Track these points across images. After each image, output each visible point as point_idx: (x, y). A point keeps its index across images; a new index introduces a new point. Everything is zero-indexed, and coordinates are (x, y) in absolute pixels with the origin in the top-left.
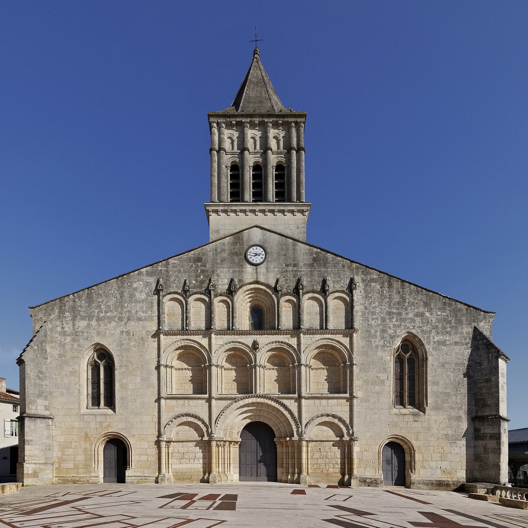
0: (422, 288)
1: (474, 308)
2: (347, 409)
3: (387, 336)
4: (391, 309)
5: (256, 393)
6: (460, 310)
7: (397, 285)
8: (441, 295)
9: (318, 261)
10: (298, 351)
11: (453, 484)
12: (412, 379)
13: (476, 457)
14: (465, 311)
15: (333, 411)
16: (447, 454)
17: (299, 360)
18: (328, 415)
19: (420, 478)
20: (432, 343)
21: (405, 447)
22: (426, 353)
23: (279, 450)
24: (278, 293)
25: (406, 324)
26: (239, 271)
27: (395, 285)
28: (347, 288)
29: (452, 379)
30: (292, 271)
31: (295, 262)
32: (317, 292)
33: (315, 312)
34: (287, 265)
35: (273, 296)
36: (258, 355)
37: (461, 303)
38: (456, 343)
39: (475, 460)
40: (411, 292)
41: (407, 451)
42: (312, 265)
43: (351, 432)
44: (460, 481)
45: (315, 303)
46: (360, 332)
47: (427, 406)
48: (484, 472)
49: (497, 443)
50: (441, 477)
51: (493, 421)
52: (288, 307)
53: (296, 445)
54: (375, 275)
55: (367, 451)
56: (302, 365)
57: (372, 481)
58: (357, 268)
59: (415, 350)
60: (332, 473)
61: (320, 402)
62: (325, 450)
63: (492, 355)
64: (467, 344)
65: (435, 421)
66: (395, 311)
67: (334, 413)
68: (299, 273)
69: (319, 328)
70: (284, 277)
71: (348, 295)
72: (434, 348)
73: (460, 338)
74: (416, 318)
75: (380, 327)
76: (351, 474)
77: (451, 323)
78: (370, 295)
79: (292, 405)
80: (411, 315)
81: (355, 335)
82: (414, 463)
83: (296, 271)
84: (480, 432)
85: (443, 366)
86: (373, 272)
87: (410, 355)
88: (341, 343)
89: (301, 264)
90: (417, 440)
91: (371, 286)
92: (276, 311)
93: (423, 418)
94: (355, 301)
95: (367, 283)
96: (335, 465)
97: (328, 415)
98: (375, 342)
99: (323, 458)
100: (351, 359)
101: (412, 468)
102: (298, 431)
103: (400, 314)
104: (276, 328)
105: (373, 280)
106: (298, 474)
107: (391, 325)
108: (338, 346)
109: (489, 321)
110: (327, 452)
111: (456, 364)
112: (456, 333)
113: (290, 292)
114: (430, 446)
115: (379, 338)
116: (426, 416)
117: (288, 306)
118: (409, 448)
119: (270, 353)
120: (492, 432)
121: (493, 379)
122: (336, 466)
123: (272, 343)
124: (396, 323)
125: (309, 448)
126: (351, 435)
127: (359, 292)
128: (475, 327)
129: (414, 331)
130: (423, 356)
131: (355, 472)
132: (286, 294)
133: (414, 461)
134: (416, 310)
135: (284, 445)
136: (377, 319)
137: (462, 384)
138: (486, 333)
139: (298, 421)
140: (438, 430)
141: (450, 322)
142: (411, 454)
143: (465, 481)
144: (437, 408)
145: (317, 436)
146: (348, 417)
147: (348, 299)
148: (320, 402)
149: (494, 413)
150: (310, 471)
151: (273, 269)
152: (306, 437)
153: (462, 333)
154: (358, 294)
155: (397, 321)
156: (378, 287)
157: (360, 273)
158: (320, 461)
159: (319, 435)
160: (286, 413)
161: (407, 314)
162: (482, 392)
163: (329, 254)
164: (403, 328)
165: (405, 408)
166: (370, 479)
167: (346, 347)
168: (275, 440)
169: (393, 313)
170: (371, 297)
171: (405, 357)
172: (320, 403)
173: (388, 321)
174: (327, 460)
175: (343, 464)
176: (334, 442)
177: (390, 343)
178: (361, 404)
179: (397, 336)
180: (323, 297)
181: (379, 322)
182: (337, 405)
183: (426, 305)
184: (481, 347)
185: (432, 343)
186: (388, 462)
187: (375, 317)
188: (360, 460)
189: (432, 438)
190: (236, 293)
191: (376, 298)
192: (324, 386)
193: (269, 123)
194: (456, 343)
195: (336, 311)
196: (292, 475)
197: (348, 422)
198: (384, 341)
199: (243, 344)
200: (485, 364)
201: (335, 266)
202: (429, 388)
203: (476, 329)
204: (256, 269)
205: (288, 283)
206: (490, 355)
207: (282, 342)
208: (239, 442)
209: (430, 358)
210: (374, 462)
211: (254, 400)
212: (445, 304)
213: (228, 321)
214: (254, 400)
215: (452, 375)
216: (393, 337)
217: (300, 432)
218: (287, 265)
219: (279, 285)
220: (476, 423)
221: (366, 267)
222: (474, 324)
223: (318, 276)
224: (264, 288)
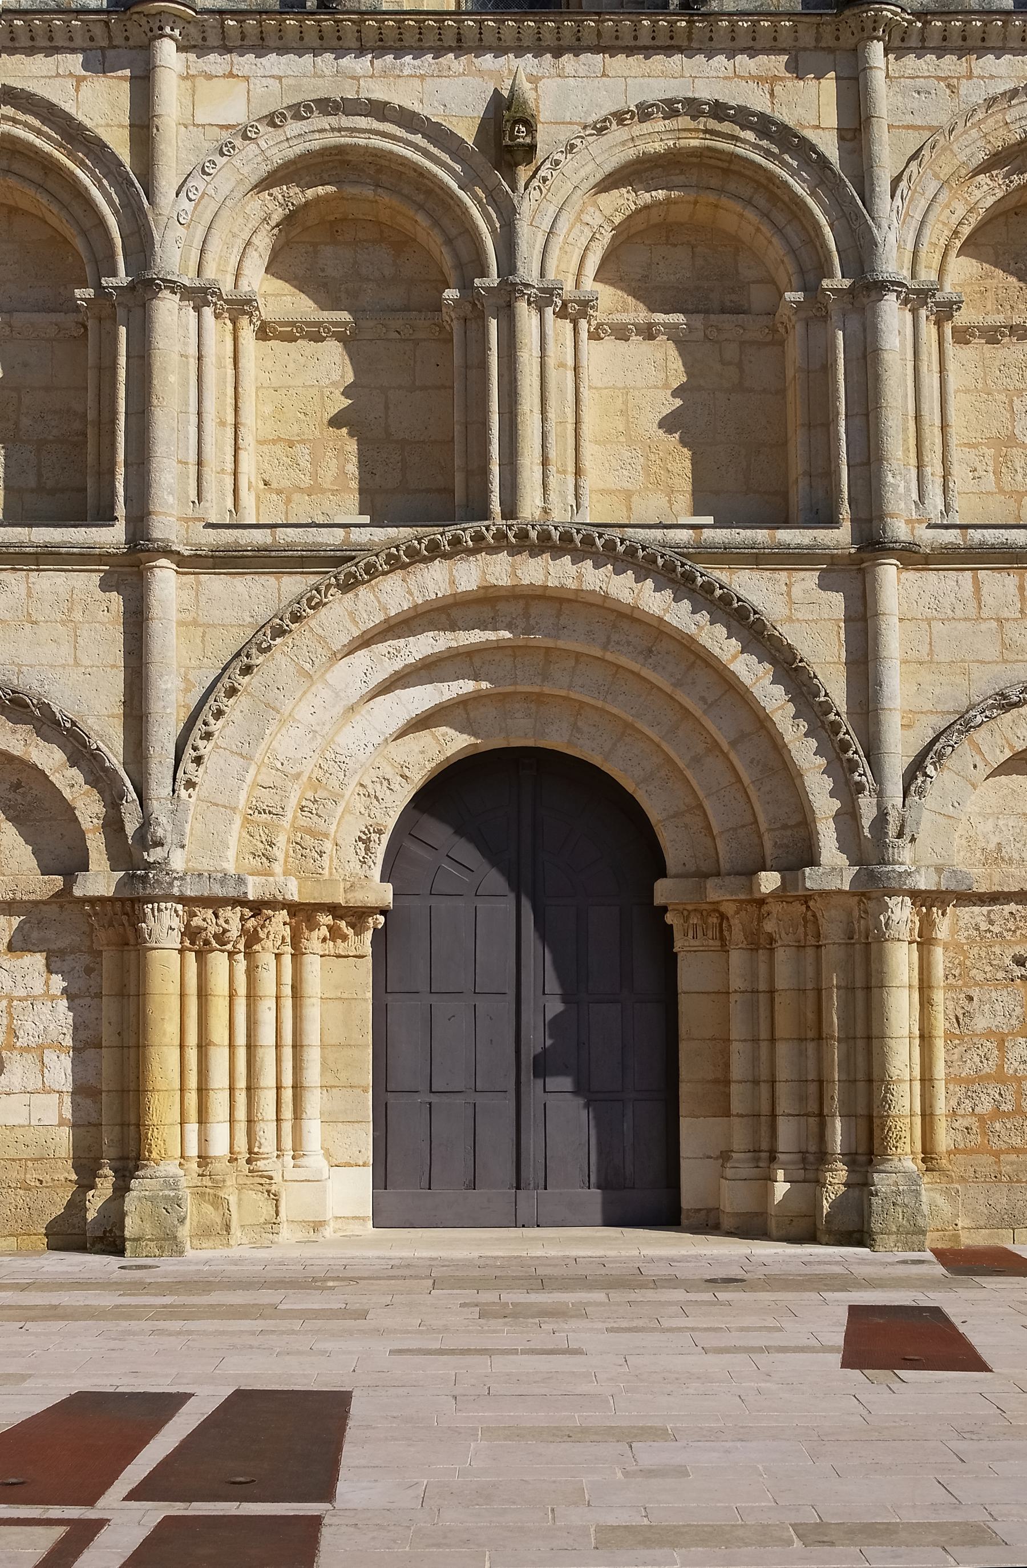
5: (510, 511)
56: (881, 287)
102: (113, 825)
106: (851, 1159)
125: (939, 954)
135: (737, 934)
145: (996, 857)
150: (944, 1140)
159: (1008, 851)
196: (800, 1174)
199: (408, 120)
217: (866, 823)
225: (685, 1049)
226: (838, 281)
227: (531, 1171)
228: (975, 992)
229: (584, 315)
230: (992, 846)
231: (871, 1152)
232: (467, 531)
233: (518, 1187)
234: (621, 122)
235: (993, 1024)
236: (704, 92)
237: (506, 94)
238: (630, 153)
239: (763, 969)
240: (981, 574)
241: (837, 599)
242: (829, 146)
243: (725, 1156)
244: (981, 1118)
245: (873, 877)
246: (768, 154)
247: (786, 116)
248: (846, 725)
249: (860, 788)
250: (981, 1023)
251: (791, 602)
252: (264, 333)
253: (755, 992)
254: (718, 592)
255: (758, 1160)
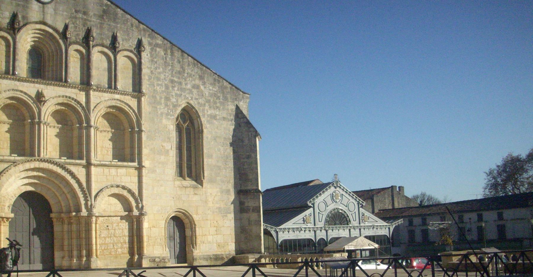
0: (198, 61)
1: (236, 88)
2: (136, 179)
3: (171, 104)
4: (173, 77)
5: (39, 156)
6: (226, 88)
7: (177, 54)
8: (211, 71)
9: (108, 14)
10: (87, 109)
11: (227, 257)
12: (189, 150)
13: (242, 229)
14: (229, 89)
15: (122, 182)
16: (221, 227)
17: (88, 121)
18: (118, 186)
19: (201, 254)
20: (206, 116)
21: (186, 221)
22: (202, 125)
23: (57, 228)
24: (67, 40)
25: (186, 94)
26: (23, 6)
27: (176, 54)
28: (135, 49)
29: (222, 153)
30: (82, 19)
31: (85, 10)
32: (107, 47)
33: (103, 68)
34: (76, 11)
35: (61, 41)
36: (44, 109)
37: (227, 81)
38: (224, 119)
39: (241, 232)
40: (189, 64)
41: (187, 225)
42: (101, 17)
43: (140, 205)
44: (231, 254)
45: (104, 58)
46: (147, 97)
47: (204, 179)
48: (249, 244)
49: (258, 215)
50: (217, 251)
51: (254, 195)
52: (75, 57)
53: (83, 221)
54: (159, 41)
55: (155, 227)
56: (91, 126)
57: (161, 260)
58: (144, 30)
59: (192, 122)
60: (120, 254)
61: (109, 171)
62: (112, 227)
63: (251, 134)
64: (231, 120)
65: (211, 194)
66: (176, 79)
67: (123, 184)
68: (88, 23)
69: (107, 86)
70: (73, 24)
71: (136, 56)
72: (208, 121)
73: (227, 114)
74: (193, 90)
75: (164, 94)
76: (141, 255)
77: (219, 99)
78: (155, 60)
79: (80, 173)
80: (189, 86)
81: (143, 99)
82: (196, 238)
83: (86, 20)
84: (244, 205)
85: (215, 139)
86: (158, 37)
87: (188, 126)
88: (129, 106)
89: (91, 14)
90: (197, 214)
91: (156, 51)
92: (64, 61)
93: (201, 191)
94: (143, 63)
95: (153, 47)
96: (123, 244)
97: (118, 186)
98: (160, 109)
99: (111, 237)
100: (139, 125)
101: (193, 244)
102: (86, 204)
103: (180, 83)
104: (64, 80)
105: (157, 45)
106: (86, 256)
107: (173, 94)
108: (127, 108)
109: (246, 101)
110: (115, 230)
111: (225, 138)
112: (223, 109)
113: (79, 42)
114: (208, 220)
115: (163, 105)
116: (204, 189)
117: (76, 57)
118: (190, 222)
119: (59, 107)
120: (254, 205)
121: (253, 155)
122: (125, 246)
123: (59, 96)
124: (177, 92)
125: (98, 225)
126: (141, 209)
127: (146, 55)
128: (237, 105)
129: (192, 102)
130: (199, 128)
131: (145, 251)
132: (76, 43)
133: (195, 236)
134: (193, 82)
135: (66, 222)
136: (161, 85)
137: (229, 159)
138: (245, 112)
139: (87, 191)
140: (213, 203)
141: (218, 98)
142: (192, 229)
143: (235, 253)
144: (211, 181)
145: (104, 211)
146: (137, 189)
147: (136, 59)
148: (109, 171)
149: (255, 188)
150: (98, 253)
151: (61, 12)
152: (96, 211)
153: (228, 110)
154: (145, 56)
155: (178, 90)
156: (162, 53)
157: (147, 36)
158: (108, 240)
159: (106, 210)
160: (73, 182)
161: (186, 84)
162: (245, 167)
163: (119, 10)
164: (183, 98)
165: (185, 180)
166: (159, 257)
167: (134, 111)
168: (52, 215)
169: (175, 82)
170: (156, 62)
171: (183, 127)
172: (110, 173)
173: (171, 88)
174: (115, 239)
175: (131, 242)
176: (89, 207)
177: (173, 112)
178: (148, 174)
179: (178, 105)
180: (113, 53)
181: (163, 89)
182: (126, 176)
183: (201, 78)
184: (243, 125)
185: (206, 116)
186: (171, 238)
187: (160, 83)
188: (149, 237)
189: (209, 212)
190: (19, 31)
191: (161, 64)
192: (108, 151)
193: (478, 257)
194: (224, 119)
195: (124, 70)
196: (77, 259)
197: (137, 193)
198: (168, 109)
199: (26, 94)
200: (246, 141)
201: (124, 23)
202: (205, 160)
203: (237, 108)
204: (43, 7)
205: (77, 31)
206: (250, 134)
207: (70, 98)
208: (10, 218)
209: (205, 131)
210: (161, 239)
211: (37, 164)
212: (215, 79)
213: (7, 62)
214: (37, 164)
215: (222, 148)
216: (175, 106)
217: (89, 206)
218: (76, 11)
219: (69, 32)
220: (241, 196)
221: (153, 30)
222: (236, 103)
223: (108, 30)
224: (50, 30)
225: (55, 241)
226: (85, 125)
227: (32, 261)
228: (102, 231)
229: (48, 125)
230: (104, 209)
231: (89, 255)
232: (33, 158)
233: (30, 264)
234: (56, 97)
235: (104, 236)
236: (68, 95)
237: (40, 91)
238: (114, 104)
239: (70, 227)
240: (104, 169)
241: (137, 172)
242: (84, 104)
243: (206, 252)
244: (102, 250)
245: (91, 214)
246: (76, 104)
247: (78, 99)
248: (86, 190)
249: (88, 200)
250: (102, 236)
251: (78, 172)
252: (50, 127)
253: (69, 231)
254: (69, 170)
255: (69, 257)
